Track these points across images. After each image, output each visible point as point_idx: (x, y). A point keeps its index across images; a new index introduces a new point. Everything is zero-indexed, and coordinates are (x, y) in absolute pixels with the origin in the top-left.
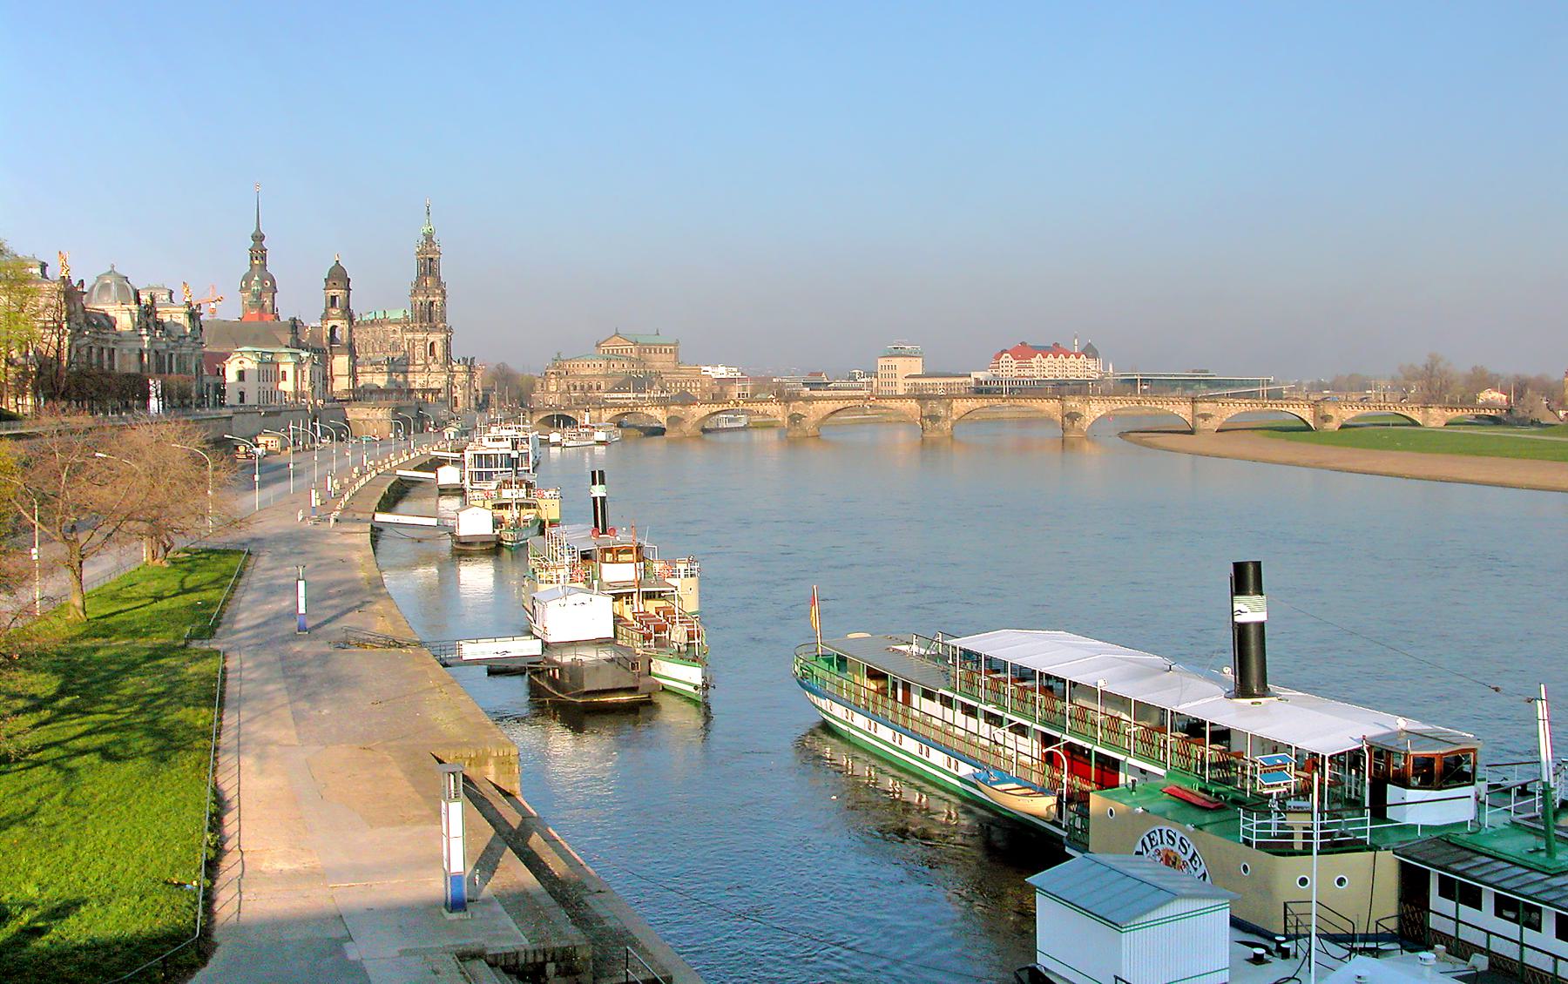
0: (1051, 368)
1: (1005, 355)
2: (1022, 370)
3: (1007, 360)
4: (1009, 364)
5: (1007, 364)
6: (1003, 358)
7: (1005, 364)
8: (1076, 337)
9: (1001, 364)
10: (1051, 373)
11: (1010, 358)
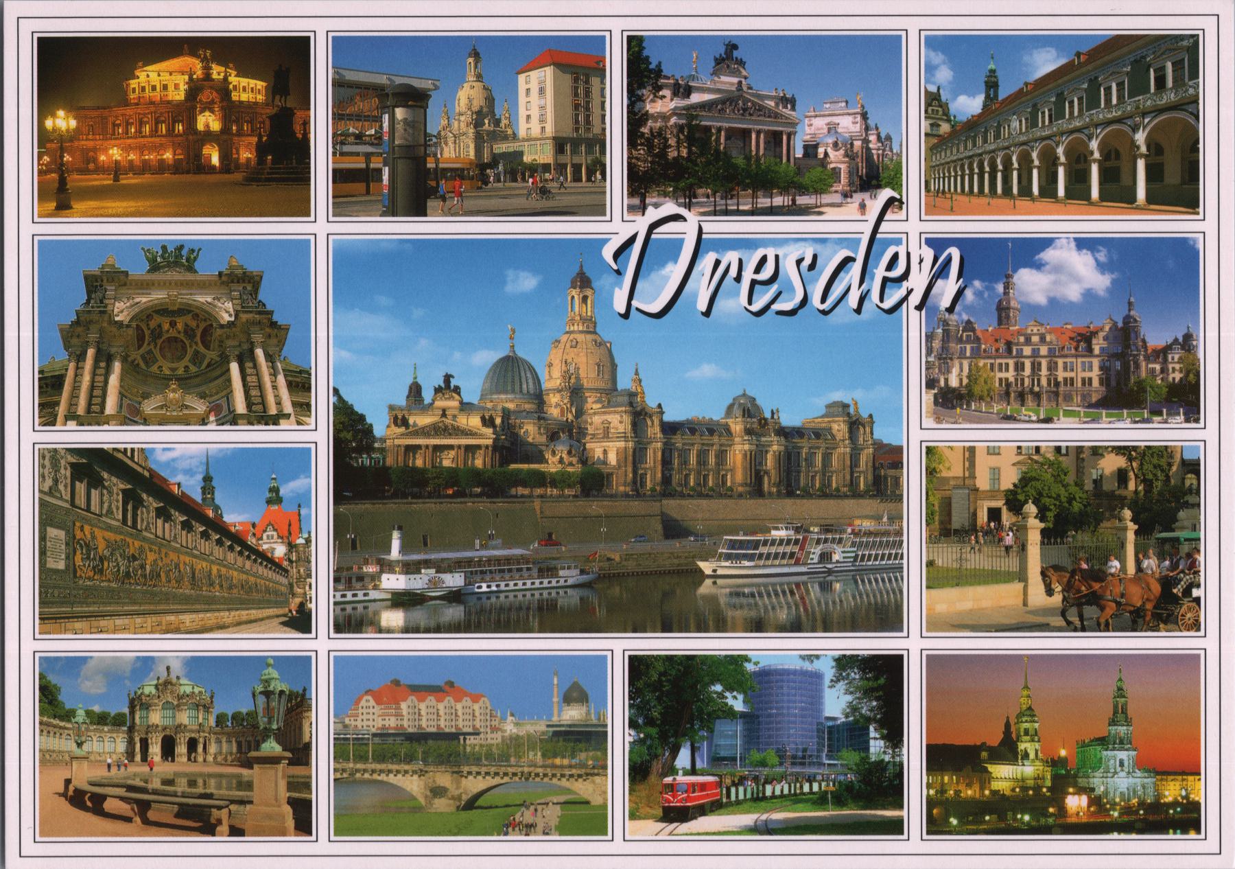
0: (431, 717)
1: (366, 697)
2: (387, 718)
3: (368, 704)
4: (371, 710)
5: (368, 711)
6: (363, 703)
7: (365, 711)
8: (556, 674)
9: (360, 711)
10: (466, 723)
11: (372, 703)
